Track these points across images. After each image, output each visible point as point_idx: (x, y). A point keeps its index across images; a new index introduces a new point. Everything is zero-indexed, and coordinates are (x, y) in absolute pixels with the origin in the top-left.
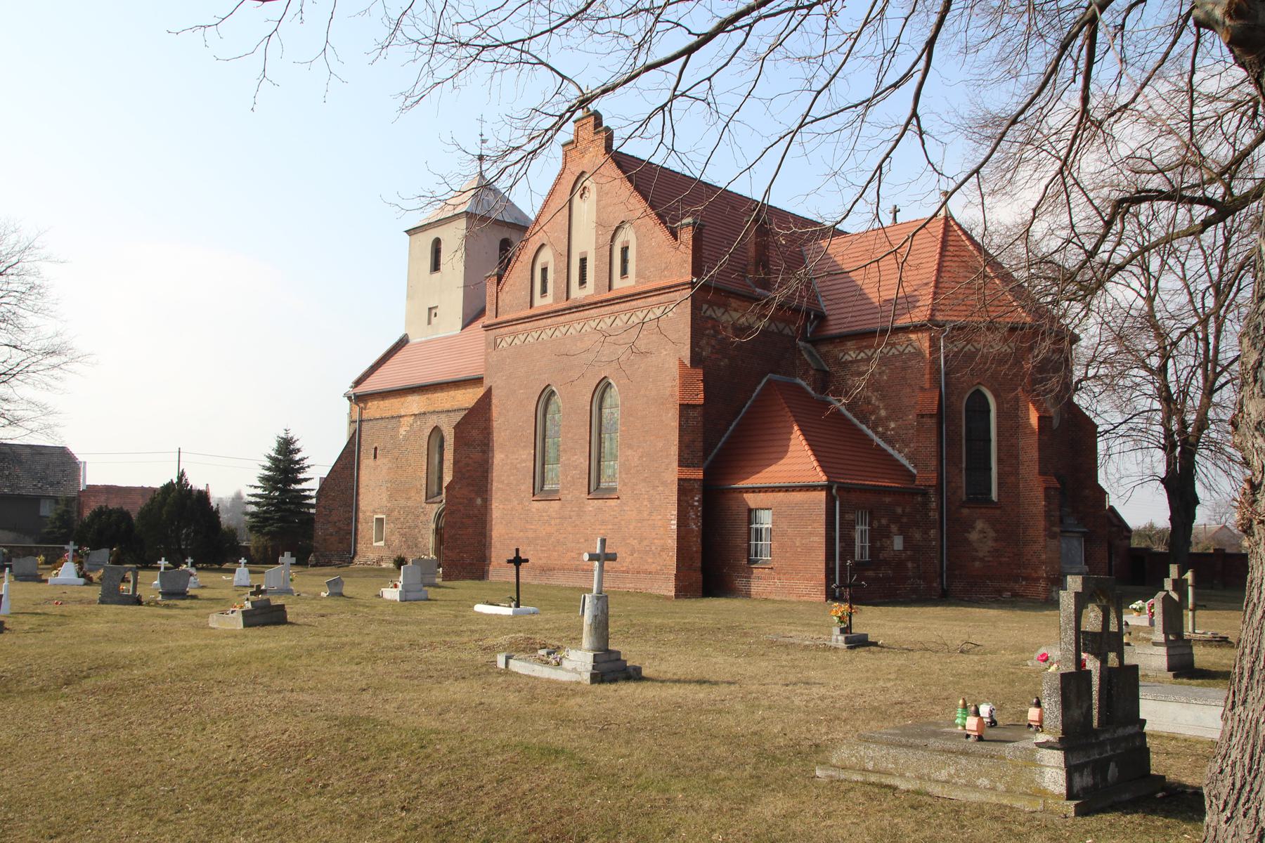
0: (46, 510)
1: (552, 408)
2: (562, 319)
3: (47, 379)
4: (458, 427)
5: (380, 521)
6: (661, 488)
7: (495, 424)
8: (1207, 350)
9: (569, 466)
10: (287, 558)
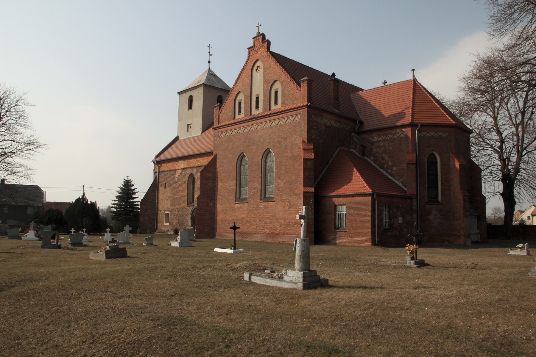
0: (30, 211)
1: (243, 163)
2: (248, 123)
3: (27, 155)
4: (202, 172)
5: (167, 214)
6: (294, 197)
7: (218, 170)
8: (518, 140)
9: (252, 189)
10: (128, 228)
